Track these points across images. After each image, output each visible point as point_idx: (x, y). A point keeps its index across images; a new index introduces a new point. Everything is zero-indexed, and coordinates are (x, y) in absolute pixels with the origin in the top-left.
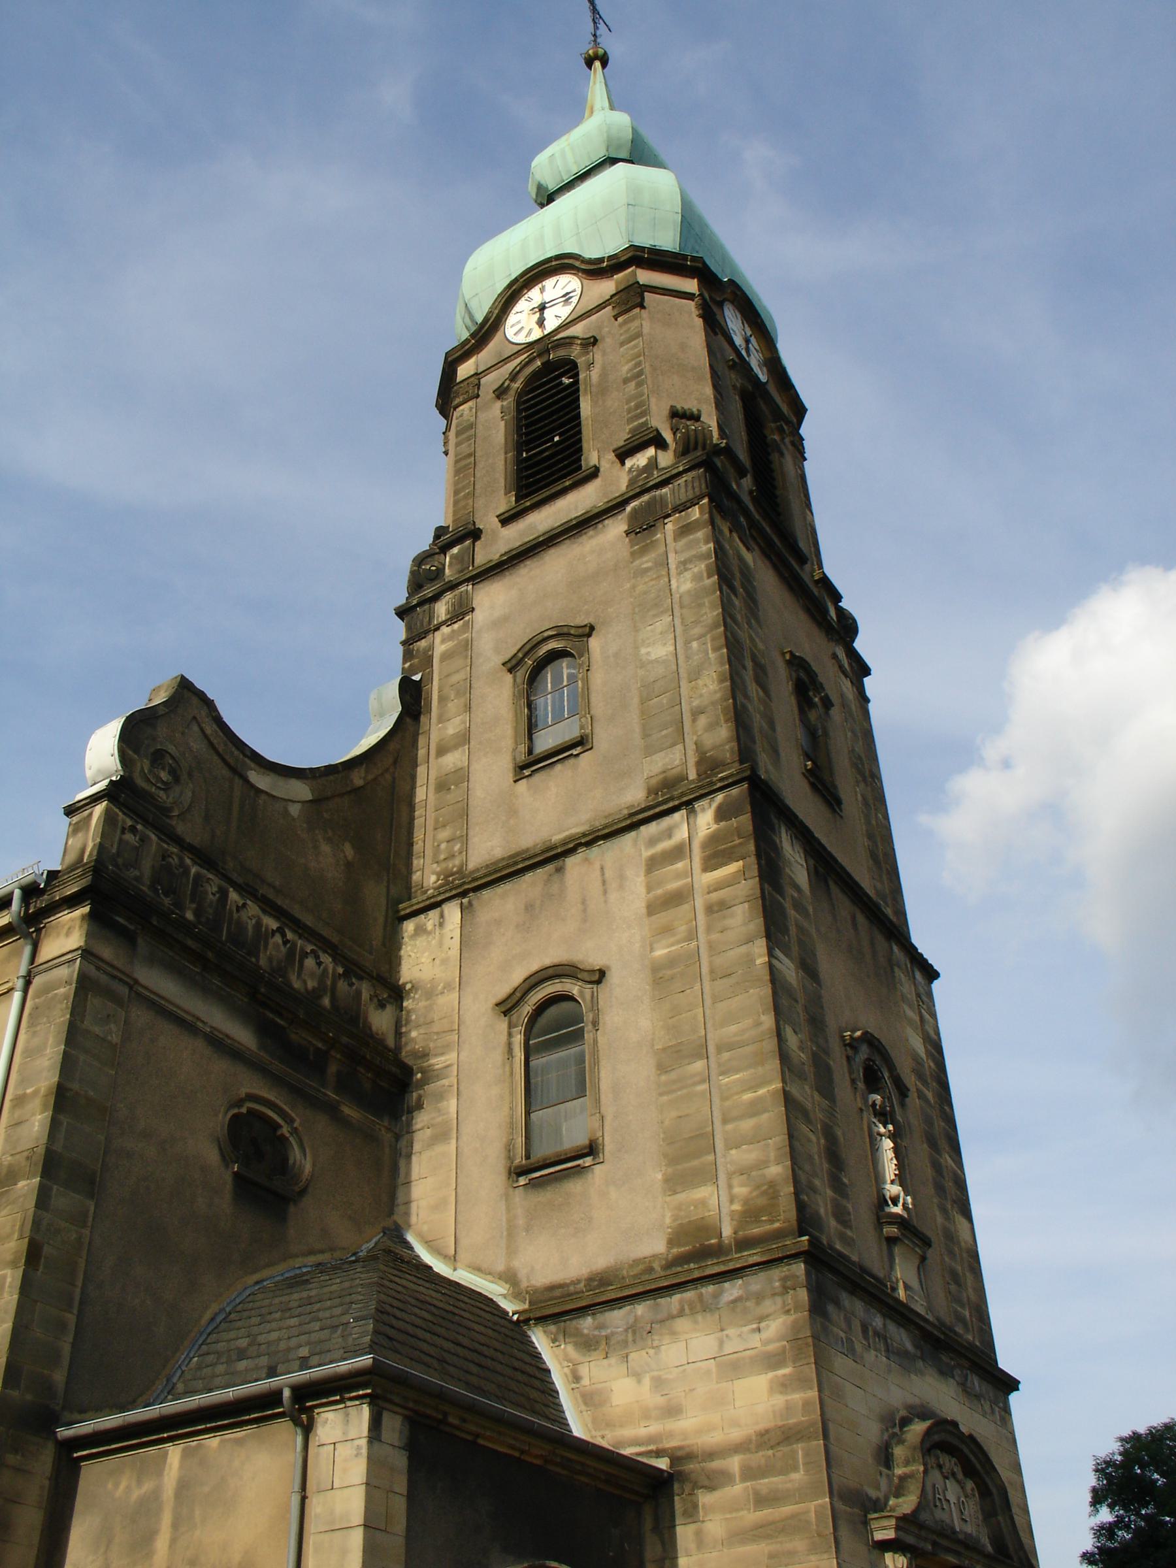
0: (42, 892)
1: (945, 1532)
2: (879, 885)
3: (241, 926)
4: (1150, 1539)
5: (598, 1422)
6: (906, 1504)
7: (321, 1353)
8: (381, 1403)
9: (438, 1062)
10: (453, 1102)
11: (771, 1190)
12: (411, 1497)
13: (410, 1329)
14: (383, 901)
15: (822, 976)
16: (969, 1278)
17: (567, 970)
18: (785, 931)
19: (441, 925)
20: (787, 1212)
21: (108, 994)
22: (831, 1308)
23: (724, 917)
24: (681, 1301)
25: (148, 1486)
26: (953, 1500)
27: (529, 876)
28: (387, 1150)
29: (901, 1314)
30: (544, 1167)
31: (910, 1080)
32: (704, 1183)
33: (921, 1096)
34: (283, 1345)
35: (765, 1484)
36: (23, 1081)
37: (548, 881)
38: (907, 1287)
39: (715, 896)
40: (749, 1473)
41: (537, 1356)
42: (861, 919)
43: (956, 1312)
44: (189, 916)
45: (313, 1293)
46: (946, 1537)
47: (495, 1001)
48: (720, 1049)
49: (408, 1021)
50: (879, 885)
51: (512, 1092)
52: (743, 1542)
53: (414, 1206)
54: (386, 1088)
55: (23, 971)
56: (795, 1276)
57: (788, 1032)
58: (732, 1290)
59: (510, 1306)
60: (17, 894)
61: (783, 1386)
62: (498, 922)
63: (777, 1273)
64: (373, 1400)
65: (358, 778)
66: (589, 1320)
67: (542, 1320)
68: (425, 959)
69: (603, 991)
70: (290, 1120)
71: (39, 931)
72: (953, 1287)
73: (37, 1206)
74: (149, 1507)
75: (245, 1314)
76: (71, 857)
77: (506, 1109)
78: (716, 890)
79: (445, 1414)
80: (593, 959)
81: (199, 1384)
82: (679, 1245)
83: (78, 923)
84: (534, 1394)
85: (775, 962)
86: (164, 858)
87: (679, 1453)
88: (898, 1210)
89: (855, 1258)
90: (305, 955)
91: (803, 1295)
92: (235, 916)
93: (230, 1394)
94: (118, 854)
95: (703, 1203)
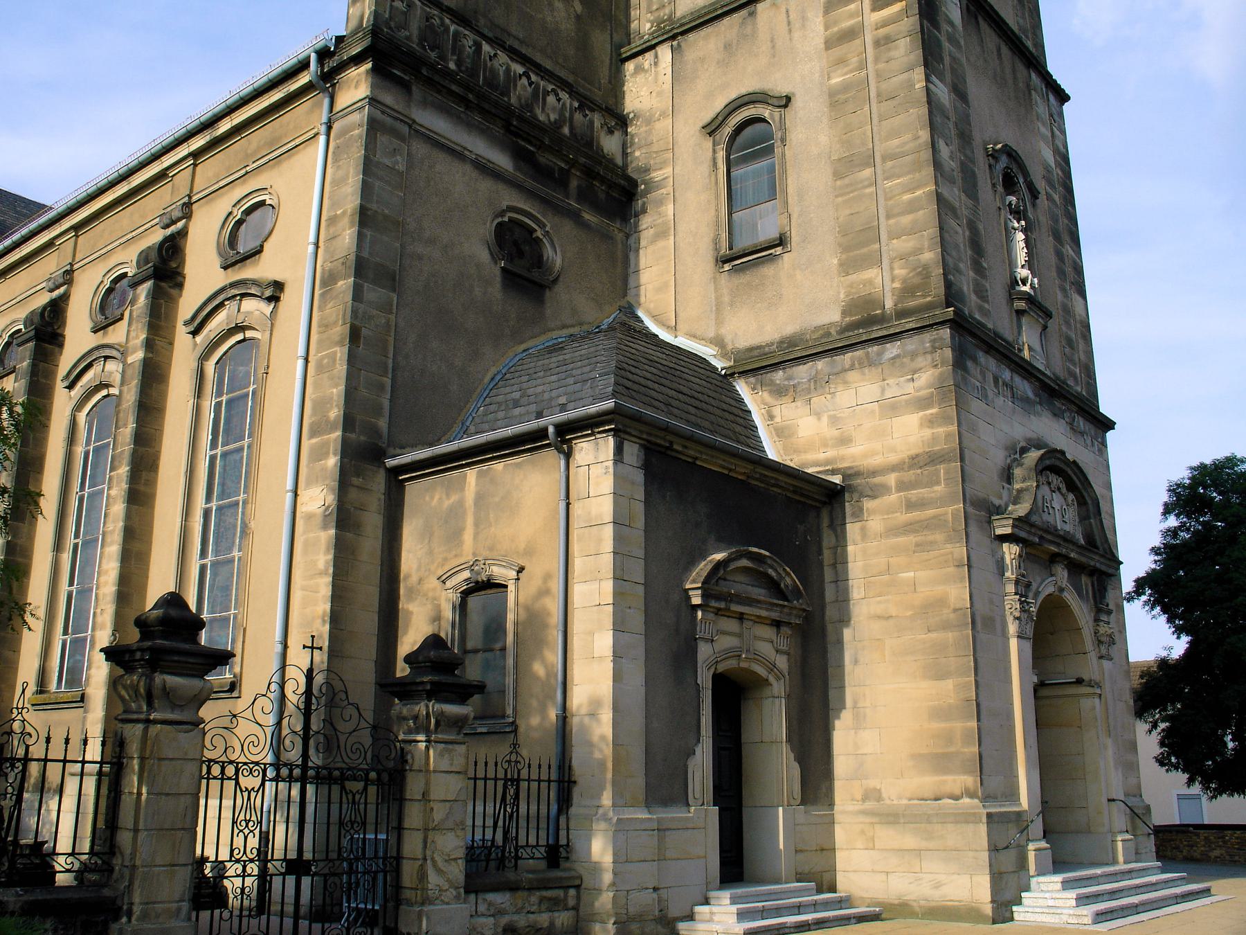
0: (333, 54)
1: (1049, 531)
2: (1021, 21)
3: (493, 72)
4: (1202, 538)
5: (786, 450)
6: (1022, 509)
7: (576, 400)
8: (623, 435)
9: (657, 175)
10: (671, 206)
11: (925, 272)
12: (647, 502)
13: (643, 381)
14: (609, 46)
15: (970, 97)
16: (1081, 346)
17: (760, 97)
18: (940, 60)
19: (656, 64)
20: (937, 289)
21: (393, 132)
22: (970, 364)
23: (889, 50)
24: (852, 359)
25: (454, 498)
26: (1057, 507)
27: (727, 20)
28: (620, 246)
29: (1025, 369)
30: (743, 256)
31: (1041, 185)
32: (870, 266)
33: (1049, 197)
34: (546, 396)
35: (914, 494)
36: (334, 205)
37: (743, 24)
38: (1030, 349)
39: (882, 32)
40: (902, 486)
41: (741, 401)
42: (1005, 50)
43: (1068, 369)
44: (452, 66)
45: (567, 357)
46: (1049, 533)
47: (702, 124)
48: (885, 158)
49: (632, 144)
50: (1021, 21)
51: (717, 197)
52: (896, 535)
53: (642, 288)
54: (618, 197)
55: (324, 119)
56: (941, 339)
57: (941, 144)
58: (892, 349)
59: (719, 364)
60: (313, 57)
61: (931, 422)
62: (702, 60)
63: (927, 336)
64: (616, 432)
66: (781, 373)
67: (743, 373)
68: (644, 92)
69: (789, 113)
70: (542, 226)
71: (333, 85)
72: (1067, 350)
73: (354, 300)
74: (456, 512)
75: (517, 374)
76: (353, 24)
77: (713, 212)
78: (882, 27)
79: (671, 443)
80: (782, 89)
81: (486, 426)
82: (851, 315)
83: (364, 77)
84: (738, 429)
85: (931, 86)
86: (427, 20)
87: (849, 472)
88: (1027, 288)
89: (990, 326)
90: (546, 93)
91: (948, 353)
92: (489, 64)
93: (509, 432)
94: (391, 17)
95: (870, 282)
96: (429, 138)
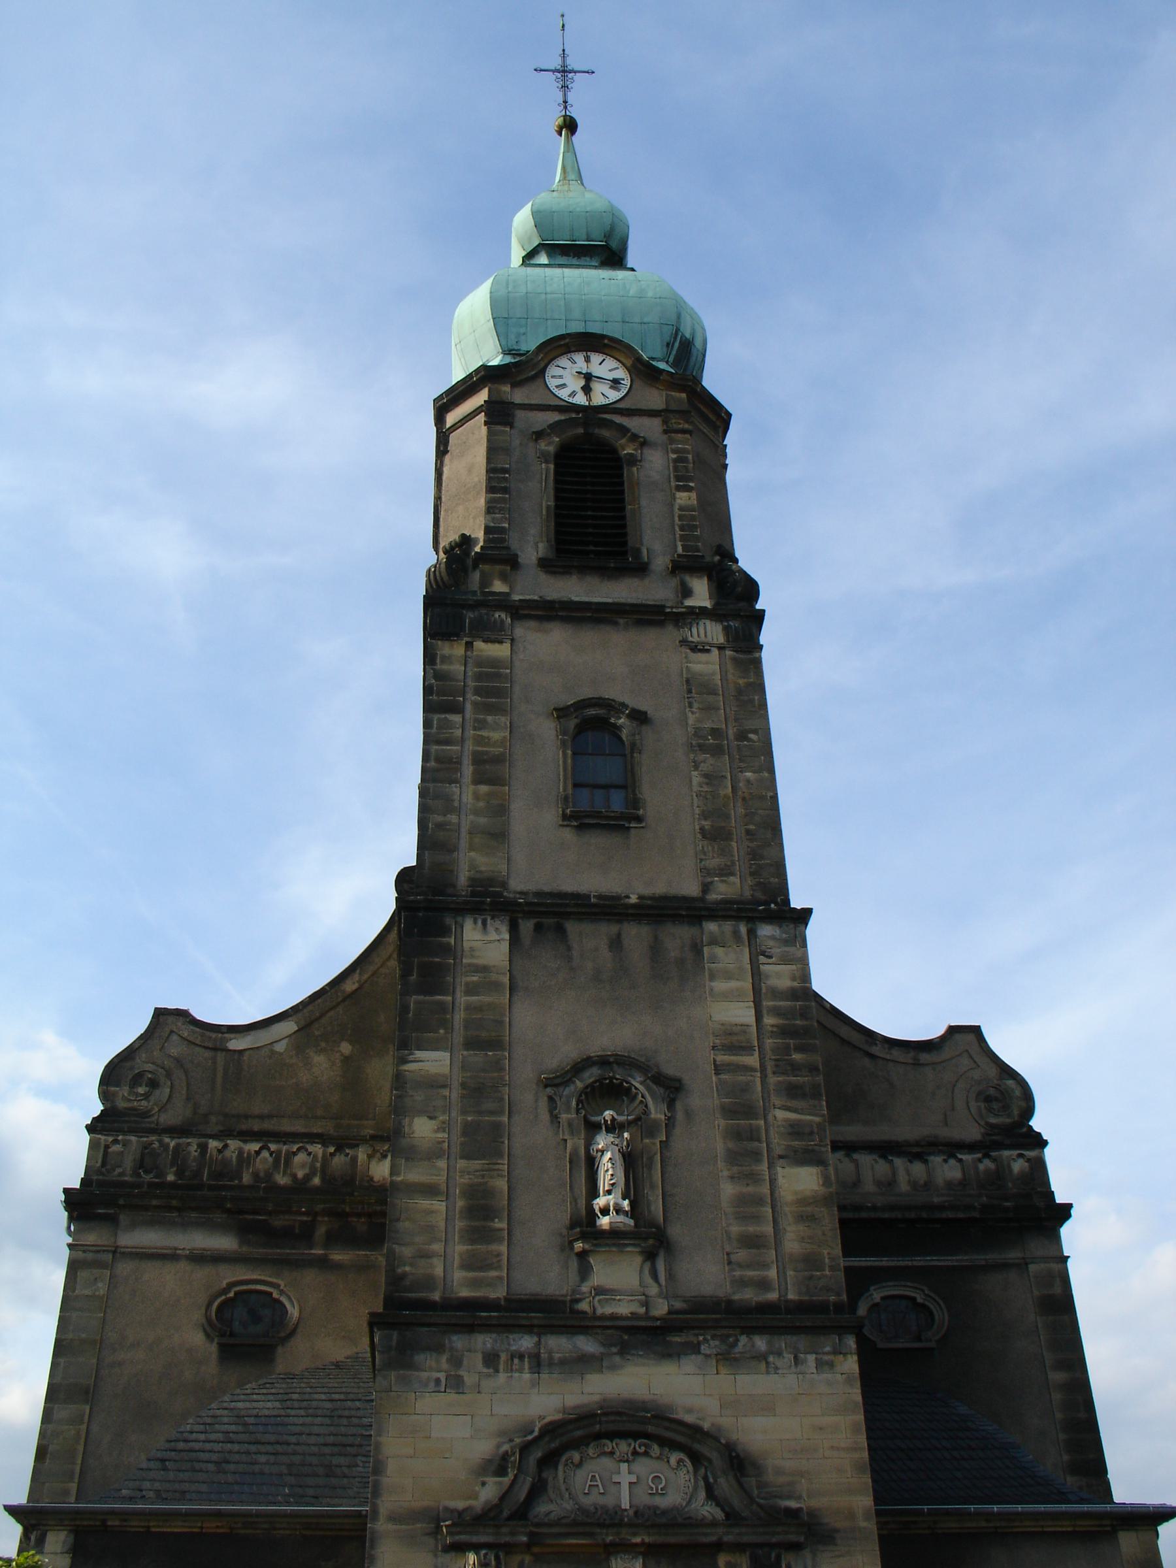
65: (350, 986)
96: (137, 1254)
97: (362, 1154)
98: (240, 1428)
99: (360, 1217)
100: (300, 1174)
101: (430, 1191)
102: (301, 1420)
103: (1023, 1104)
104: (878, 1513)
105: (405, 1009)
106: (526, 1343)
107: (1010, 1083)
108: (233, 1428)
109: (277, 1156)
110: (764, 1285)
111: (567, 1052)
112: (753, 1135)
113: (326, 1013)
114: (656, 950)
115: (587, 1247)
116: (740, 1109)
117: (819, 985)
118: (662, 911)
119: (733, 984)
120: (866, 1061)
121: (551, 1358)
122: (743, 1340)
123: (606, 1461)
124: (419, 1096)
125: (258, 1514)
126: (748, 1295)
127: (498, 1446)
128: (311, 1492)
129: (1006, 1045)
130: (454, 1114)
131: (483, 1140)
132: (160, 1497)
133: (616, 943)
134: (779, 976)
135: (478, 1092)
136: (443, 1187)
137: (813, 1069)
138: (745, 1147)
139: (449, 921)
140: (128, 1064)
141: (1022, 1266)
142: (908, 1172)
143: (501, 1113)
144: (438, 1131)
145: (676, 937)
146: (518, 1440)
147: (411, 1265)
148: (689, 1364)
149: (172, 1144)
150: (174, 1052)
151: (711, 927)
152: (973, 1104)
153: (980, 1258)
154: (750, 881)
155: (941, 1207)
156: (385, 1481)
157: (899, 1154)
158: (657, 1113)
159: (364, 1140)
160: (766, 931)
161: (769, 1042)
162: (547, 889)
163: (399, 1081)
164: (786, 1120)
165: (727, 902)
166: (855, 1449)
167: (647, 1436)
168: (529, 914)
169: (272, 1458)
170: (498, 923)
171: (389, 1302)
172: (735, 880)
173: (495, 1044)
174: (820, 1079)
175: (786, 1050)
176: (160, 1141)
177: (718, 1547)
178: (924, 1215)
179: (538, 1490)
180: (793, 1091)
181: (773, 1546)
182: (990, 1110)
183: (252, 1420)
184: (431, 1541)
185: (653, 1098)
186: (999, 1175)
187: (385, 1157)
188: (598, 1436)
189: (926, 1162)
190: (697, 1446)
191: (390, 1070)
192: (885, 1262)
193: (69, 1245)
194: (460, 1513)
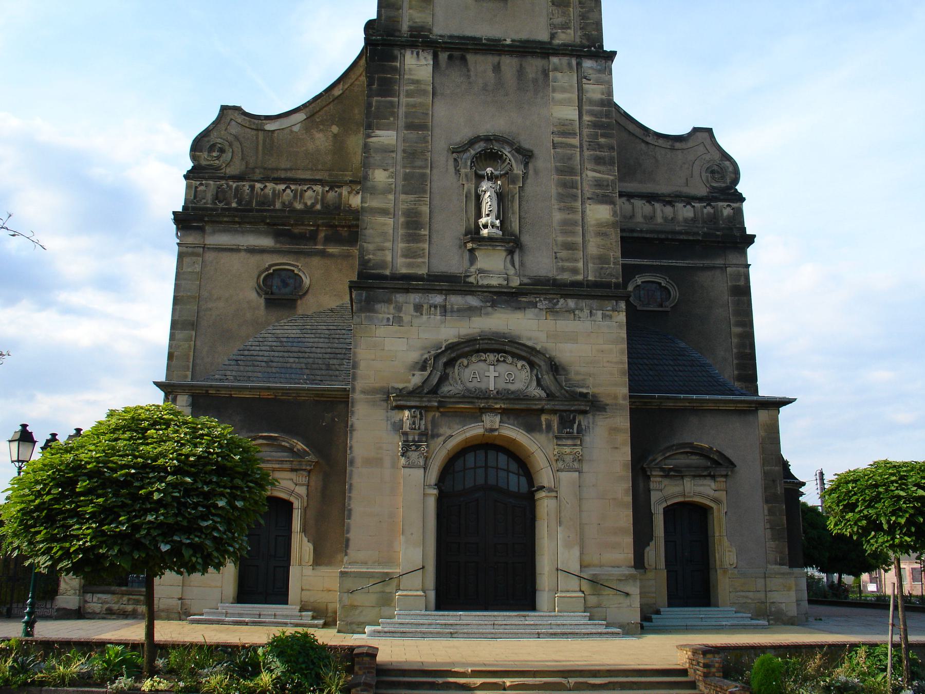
3: (265, 196)
65: (337, 92)
97: (345, 191)
98: (279, 344)
99: (344, 227)
100: (309, 203)
101: (384, 212)
102: (312, 340)
103: (733, 176)
104: (630, 397)
105: (369, 105)
106: (438, 299)
107: (727, 163)
108: (275, 344)
109: (295, 192)
110: (575, 271)
111: (466, 134)
112: (573, 185)
113: (324, 107)
114: (521, 72)
115: (474, 246)
116: (566, 170)
117: (618, 99)
118: (526, 49)
119: (566, 95)
120: (643, 145)
121: (452, 308)
122: (562, 301)
123: (481, 364)
124: (378, 157)
125: (290, 389)
126: (566, 277)
127: (422, 355)
128: (319, 378)
129: (725, 141)
130: (398, 168)
131: (416, 184)
132: (236, 379)
133: (497, 68)
134: (594, 92)
135: (411, 155)
136: (392, 210)
137: (611, 148)
138: (568, 192)
139: (396, 52)
140: (206, 139)
141: (723, 268)
142: (662, 211)
143: (426, 167)
144: (389, 177)
145: (533, 65)
146: (433, 352)
147: (373, 254)
148: (530, 313)
149: (234, 185)
150: (233, 131)
151: (555, 60)
152: (704, 174)
153: (699, 263)
154: (579, 33)
155: (680, 233)
156: (359, 372)
157: (658, 201)
158: (518, 170)
159: (346, 183)
160: (588, 64)
161: (586, 131)
162: (456, 34)
163: (366, 148)
164: (593, 177)
165: (565, 45)
166: (622, 363)
167: (505, 352)
168: (445, 49)
169: (297, 360)
170: (426, 54)
171: (360, 275)
172: (571, 32)
173: (423, 127)
174: (615, 154)
175: (596, 136)
176: (227, 184)
177: (542, 411)
178: (670, 237)
179: (443, 379)
180: (598, 161)
181: (571, 411)
182: (713, 178)
183: (285, 340)
184: (385, 404)
185: (516, 161)
186: (714, 218)
187: (358, 193)
188: (478, 351)
189: (673, 206)
190: (532, 358)
191: (361, 142)
192: (645, 262)
193: (178, 244)
194: (401, 390)
